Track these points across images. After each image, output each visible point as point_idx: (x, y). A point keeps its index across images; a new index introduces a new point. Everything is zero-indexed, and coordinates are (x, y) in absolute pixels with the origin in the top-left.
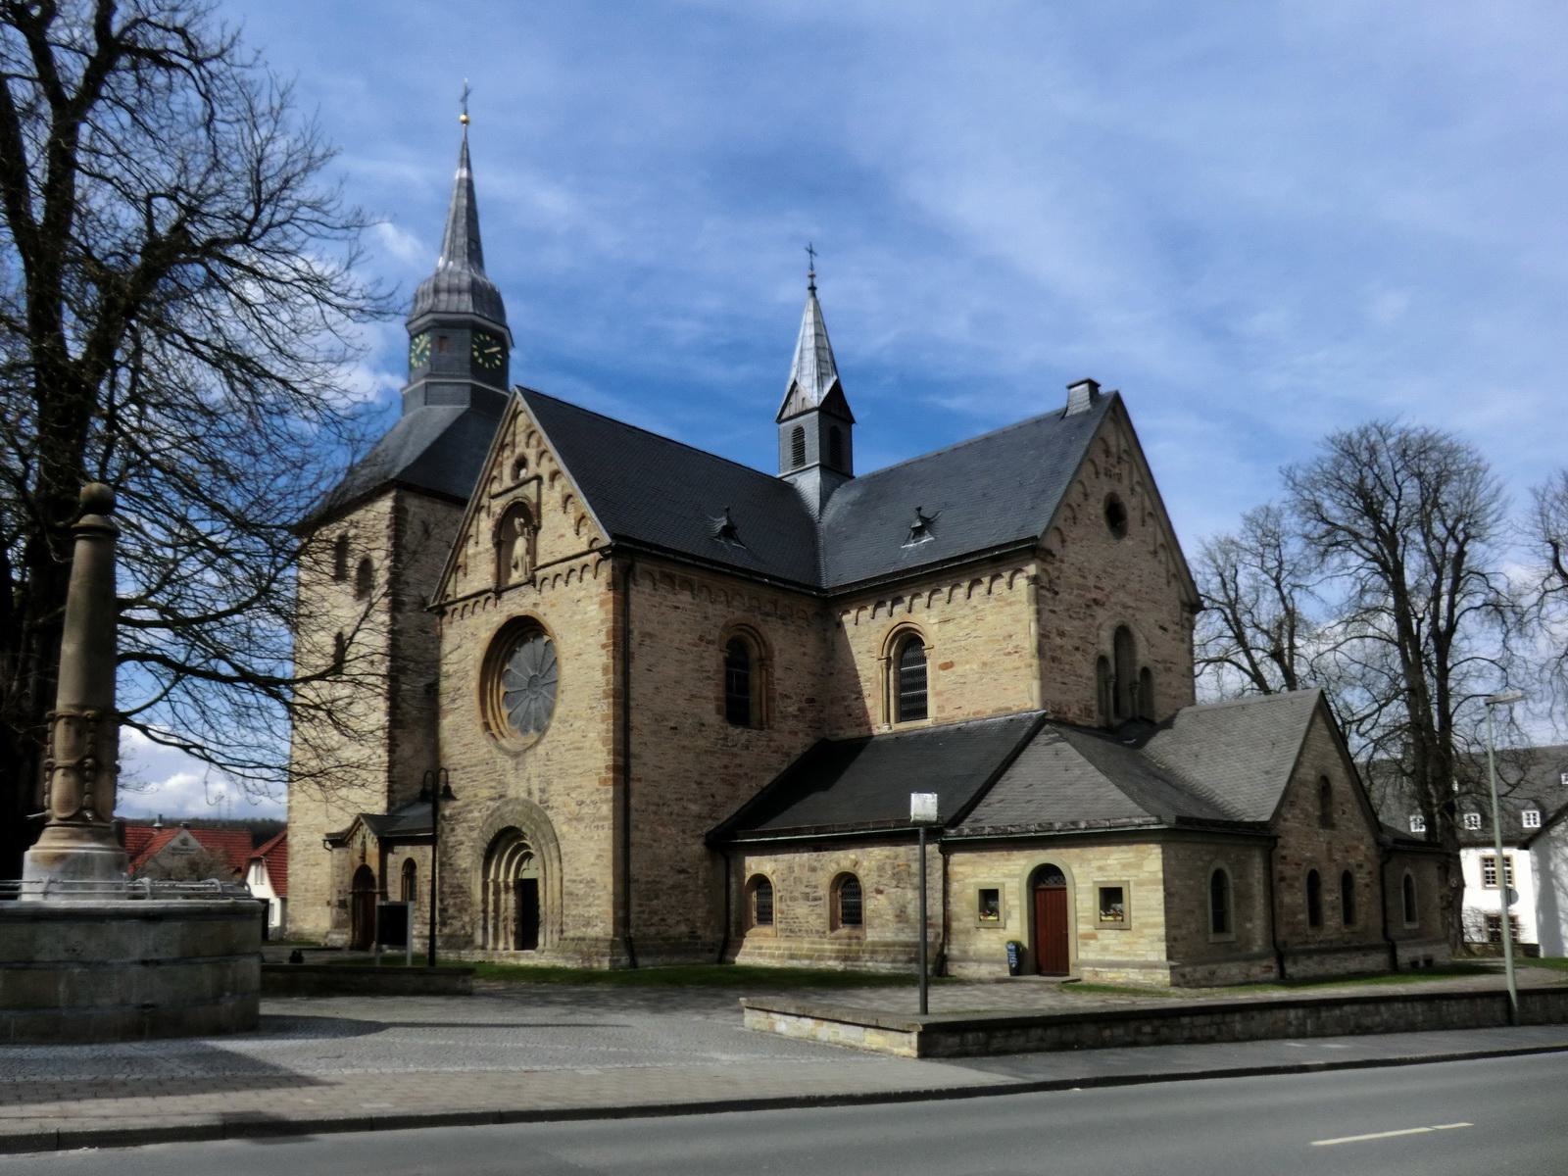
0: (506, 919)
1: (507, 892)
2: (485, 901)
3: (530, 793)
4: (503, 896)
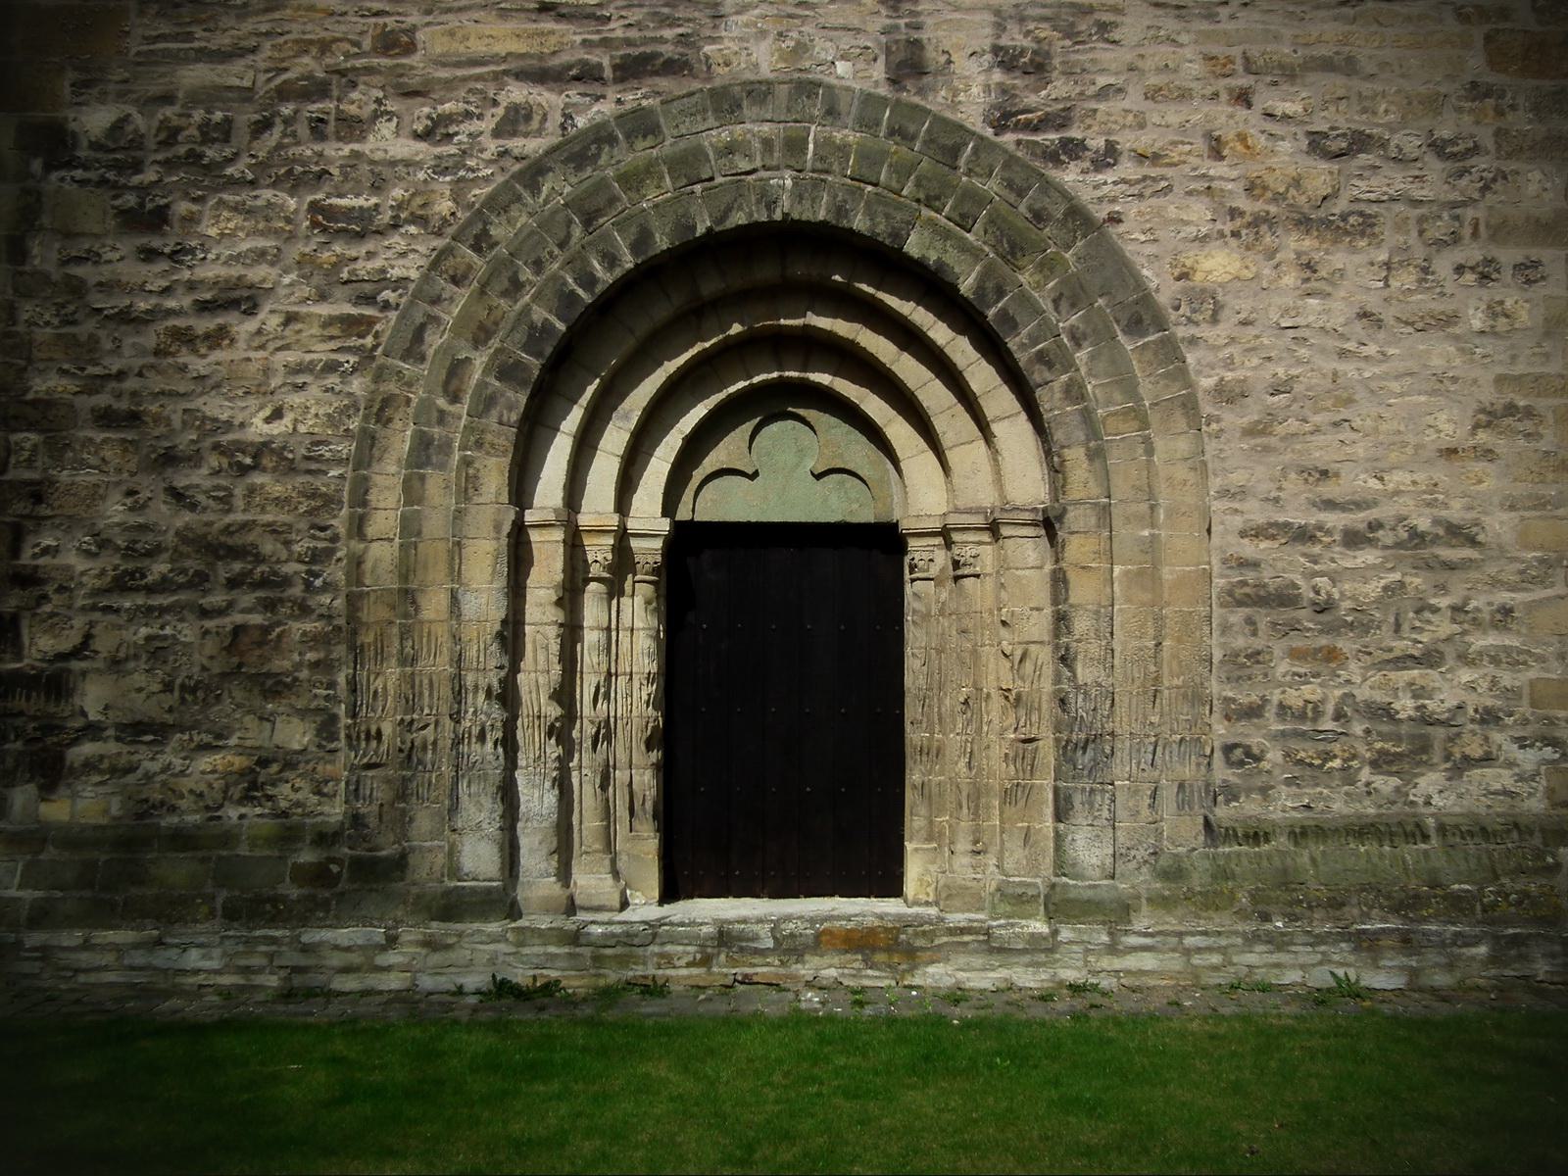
0: (605, 733)
1: (615, 590)
2: (511, 636)
3: (910, 64)
4: (593, 611)
